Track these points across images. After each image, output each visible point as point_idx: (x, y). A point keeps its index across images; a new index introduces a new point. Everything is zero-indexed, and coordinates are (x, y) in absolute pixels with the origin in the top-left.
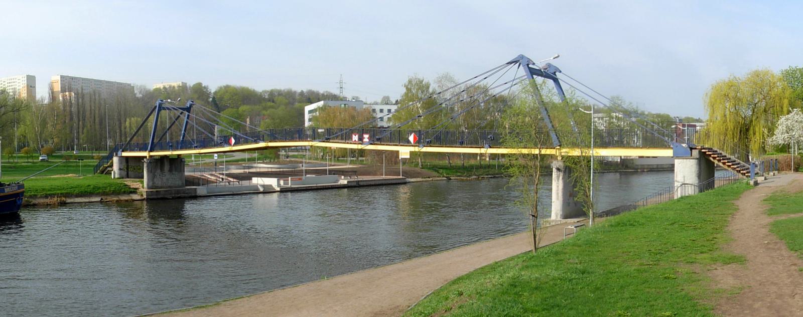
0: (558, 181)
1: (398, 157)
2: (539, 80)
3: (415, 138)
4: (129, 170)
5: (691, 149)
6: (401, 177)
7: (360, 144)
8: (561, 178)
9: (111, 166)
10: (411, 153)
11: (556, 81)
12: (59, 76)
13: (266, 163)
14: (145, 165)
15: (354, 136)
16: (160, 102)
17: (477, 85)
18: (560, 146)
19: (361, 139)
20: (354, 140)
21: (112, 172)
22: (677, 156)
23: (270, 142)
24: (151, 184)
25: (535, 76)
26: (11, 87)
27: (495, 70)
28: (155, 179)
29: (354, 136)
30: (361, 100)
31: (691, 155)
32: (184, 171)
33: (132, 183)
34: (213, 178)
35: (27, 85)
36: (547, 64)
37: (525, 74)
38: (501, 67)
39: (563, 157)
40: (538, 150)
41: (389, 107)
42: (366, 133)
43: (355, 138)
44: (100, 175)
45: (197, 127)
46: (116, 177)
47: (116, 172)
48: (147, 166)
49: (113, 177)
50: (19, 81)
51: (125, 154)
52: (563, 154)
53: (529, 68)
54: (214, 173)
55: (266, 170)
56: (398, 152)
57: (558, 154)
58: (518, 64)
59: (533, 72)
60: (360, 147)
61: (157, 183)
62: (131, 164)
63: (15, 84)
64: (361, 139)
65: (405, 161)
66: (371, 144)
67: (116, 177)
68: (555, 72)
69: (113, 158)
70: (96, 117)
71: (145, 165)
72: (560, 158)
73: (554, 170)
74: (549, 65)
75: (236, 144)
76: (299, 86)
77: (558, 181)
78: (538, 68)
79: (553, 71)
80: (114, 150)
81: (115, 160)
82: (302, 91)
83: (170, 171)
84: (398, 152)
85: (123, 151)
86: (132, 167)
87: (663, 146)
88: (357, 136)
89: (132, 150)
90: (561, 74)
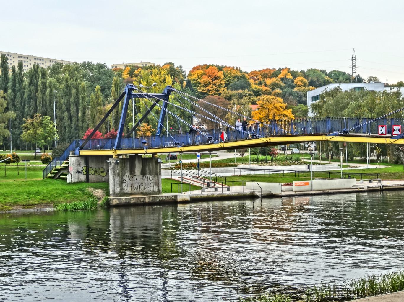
4: (90, 173)
20: (380, 133)
26: (333, 284)
28: (124, 185)
30: (380, 81)
51: (84, 153)
55: (262, 173)
56: (176, 197)
60: (389, 141)
61: (125, 189)
62: (92, 165)
64: (390, 131)
70: (401, 260)
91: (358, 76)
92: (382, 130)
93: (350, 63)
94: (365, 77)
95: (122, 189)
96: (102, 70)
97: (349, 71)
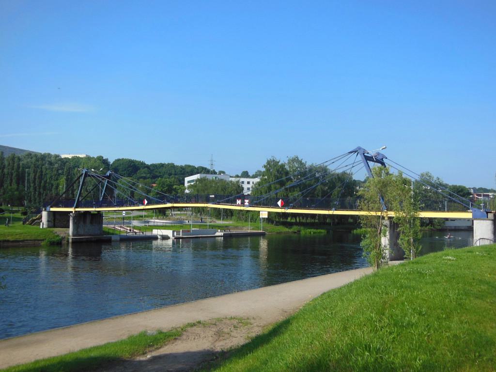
2: (371, 163)
3: (282, 203)
5: (487, 213)
6: (262, 231)
9: (41, 217)
10: (269, 213)
13: (160, 219)
14: (71, 218)
15: (238, 201)
16: (86, 170)
18: (387, 210)
19: (243, 204)
21: (41, 223)
22: (475, 217)
24: (75, 232)
27: (359, 163)
28: (79, 230)
29: (238, 201)
32: (102, 224)
33: (59, 231)
34: (122, 229)
37: (361, 159)
38: (345, 155)
40: (380, 213)
41: (248, 180)
43: (239, 202)
44: (29, 226)
47: (44, 223)
49: (41, 227)
51: (52, 209)
52: (389, 216)
53: (365, 156)
54: (122, 225)
56: (259, 212)
57: (385, 216)
58: (357, 153)
59: (368, 159)
60: (242, 208)
62: (58, 217)
67: (45, 226)
68: (382, 159)
69: (42, 211)
72: (386, 218)
74: (378, 154)
75: (148, 204)
76: (180, 161)
78: (370, 156)
79: (381, 158)
81: (44, 214)
82: (107, 159)
83: (91, 223)
84: (259, 212)
85: (51, 207)
86: (58, 220)
87: (465, 209)
88: (240, 201)
89: (57, 206)
91: (214, 170)
92: (239, 202)
93: (210, 163)
94: (217, 171)
95: (89, 176)
96: (57, 158)
97: (209, 167)
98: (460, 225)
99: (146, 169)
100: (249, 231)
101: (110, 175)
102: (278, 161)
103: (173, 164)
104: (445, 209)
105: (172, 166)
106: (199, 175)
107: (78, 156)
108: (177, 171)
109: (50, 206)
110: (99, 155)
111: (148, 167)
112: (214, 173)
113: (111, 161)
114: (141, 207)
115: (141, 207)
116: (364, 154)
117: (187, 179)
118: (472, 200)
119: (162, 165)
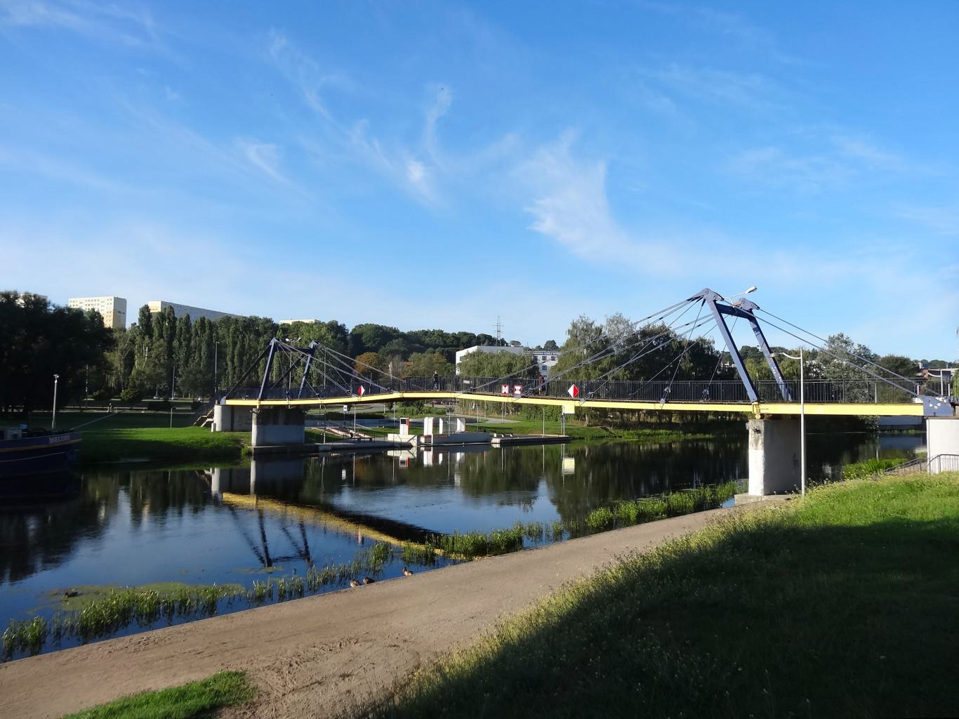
0: (757, 446)
1: (561, 412)
2: (729, 319)
6: (564, 436)
7: (510, 397)
8: (760, 442)
10: (577, 408)
11: (752, 319)
12: (160, 302)
14: (254, 416)
15: (503, 387)
17: (390, 453)
19: (512, 391)
20: (503, 392)
21: (212, 424)
23: (406, 392)
25: (724, 315)
29: (503, 387)
31: (954, 415)
35: (114, 310)
36: (740, 300)
37: (711, 312)
38: (680, 305)
39: (762, 416)
42: (519, 385)
43: (505, 389)
45: (329, 378)
46: (217, 429)
48: (258, 418)
49: (212, 431)
50: (103, 304)
51: (230, 402)
52: (762, 412)
53: (717, 305)
56: (528, 418)
57: (755, 412)
58: (702, 300)
59: (721, 309)
60: (510, 400)
63: (97, 302)
65: (568, 416)
66: (523, 397)
67: (217, 429)
68: (751, 309)
71: (254, 416)
72: (758, 417)
73: (751, 432)
75: (366, 394)
77: (757, 446)
78: (729, 305)
80: (215, 397)
81: (217, 409)
86: (235, 418)
88: (507, 387)
90: (759, 311)
92: (505, 389)
97: (494, 335)
98: (338, 595)
99: (401, 339)
100: (543, 435)
101: (315, 347)
102: (591, 322)
103: (266, 319)
104: (874, 398)
105: (441, 334)
106: (476, 347)
107: (300, 321)
108: (448, 341)
109: (225, 397)
110: (331, 320)
111: (403, 335)
112: (502, 343)
113: (350, 328)
114: (354, 399)
115: (354, 399)
116: (715, 301)
117: (460, 354)
118: (921, 381)
119: (426, 333)
